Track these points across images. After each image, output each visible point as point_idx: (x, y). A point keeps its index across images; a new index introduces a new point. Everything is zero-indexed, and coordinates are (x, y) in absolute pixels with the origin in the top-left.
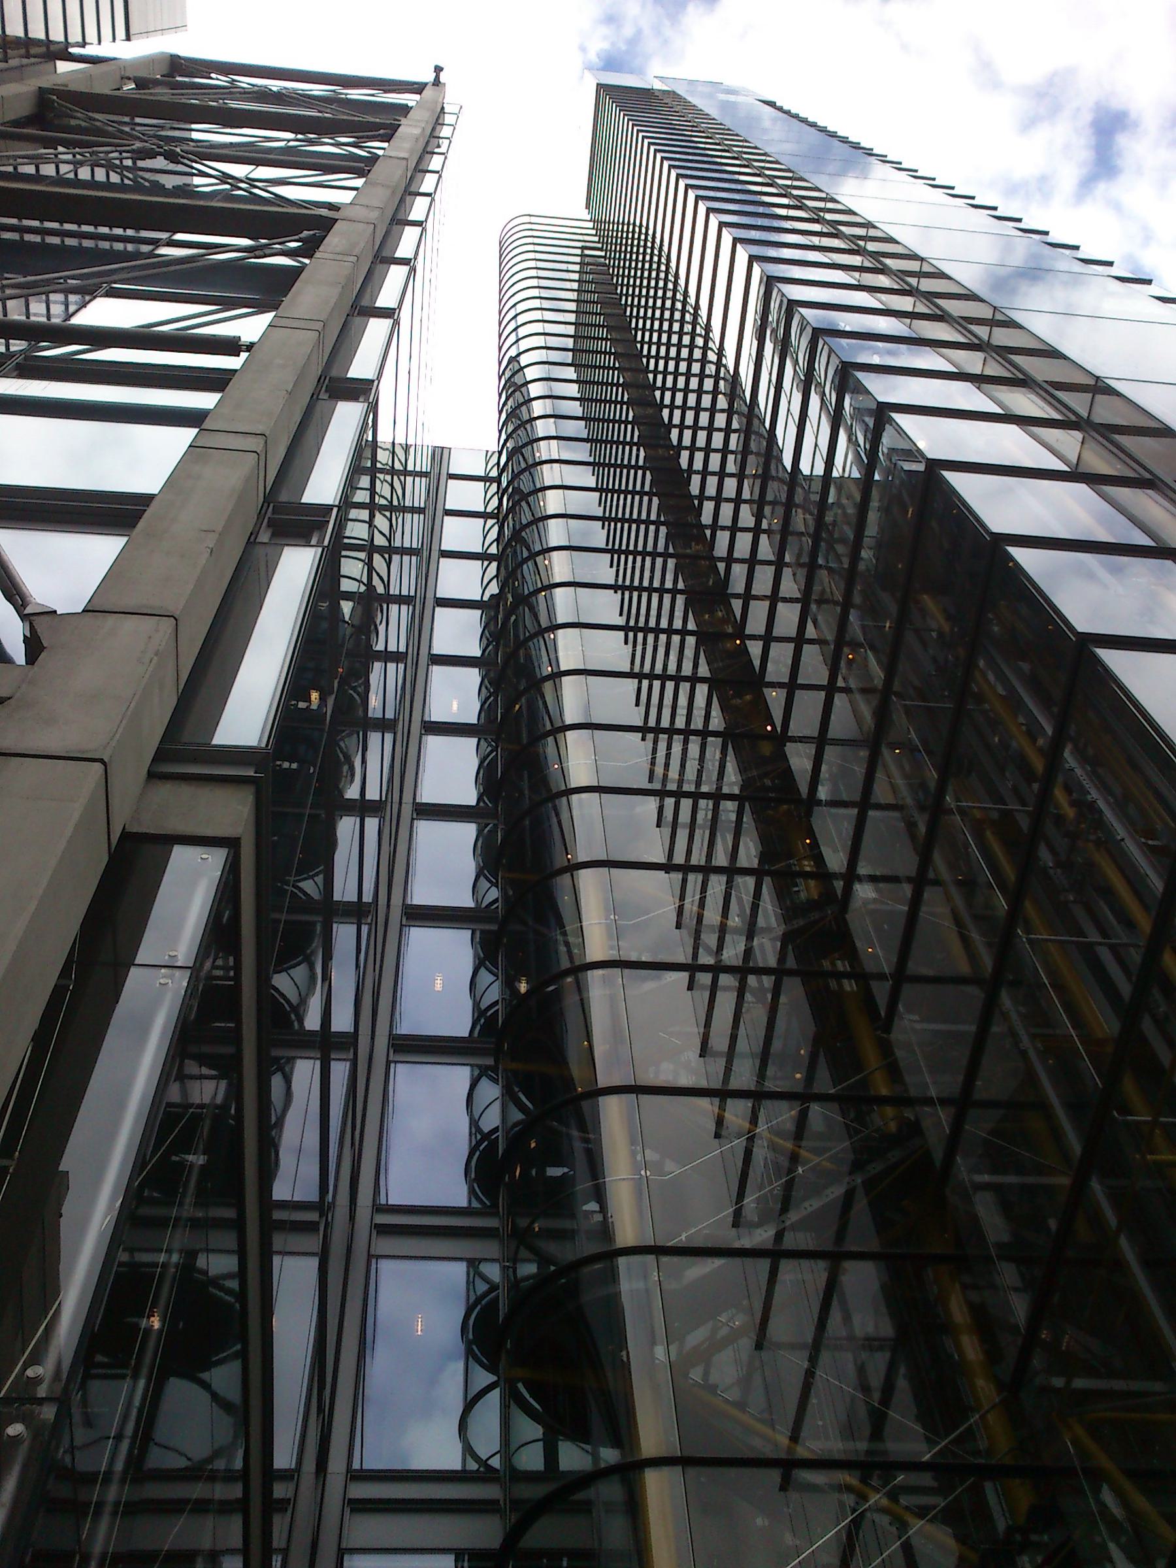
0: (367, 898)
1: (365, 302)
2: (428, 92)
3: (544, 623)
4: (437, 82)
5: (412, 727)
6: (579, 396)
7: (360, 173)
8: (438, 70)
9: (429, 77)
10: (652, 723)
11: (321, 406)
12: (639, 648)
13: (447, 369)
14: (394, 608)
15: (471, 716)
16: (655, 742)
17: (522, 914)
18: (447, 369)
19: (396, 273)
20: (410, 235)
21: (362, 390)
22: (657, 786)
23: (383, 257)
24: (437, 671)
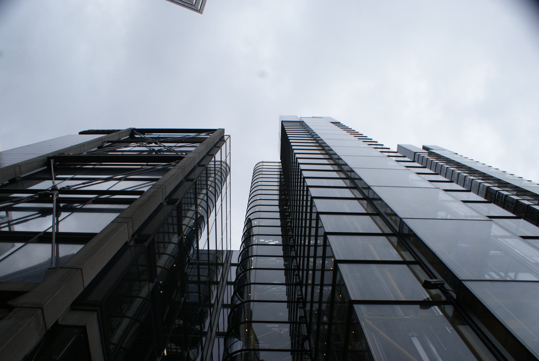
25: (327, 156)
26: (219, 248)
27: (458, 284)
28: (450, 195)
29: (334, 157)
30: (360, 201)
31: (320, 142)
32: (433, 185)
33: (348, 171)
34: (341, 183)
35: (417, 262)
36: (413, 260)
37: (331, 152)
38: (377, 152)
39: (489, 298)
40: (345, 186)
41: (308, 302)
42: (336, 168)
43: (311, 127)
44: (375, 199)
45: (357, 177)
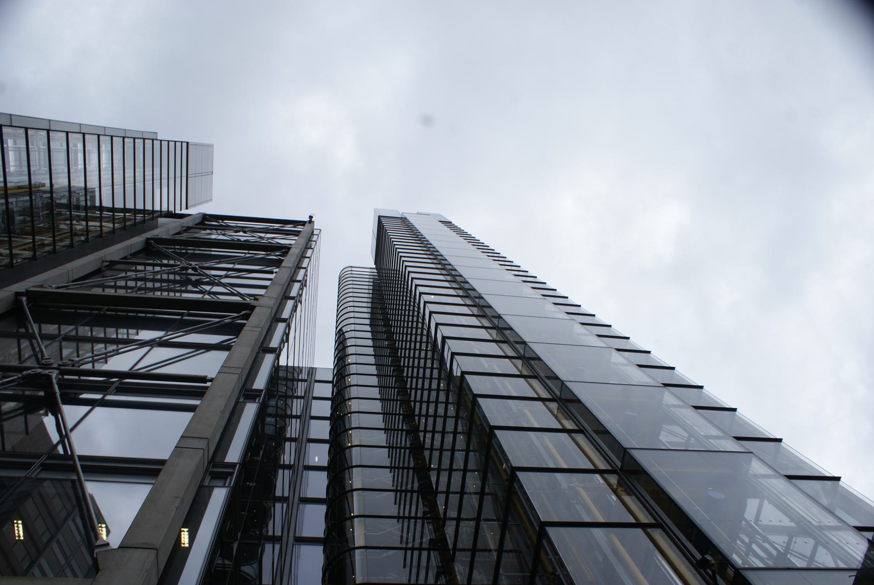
0: (292, 463)
1: (277, 316)
2: (307, 224)
3: (347, 427)
4: (311, 222)
5: (303, 441)
6: (379, 397)
7: (297, 235)
8: (311, 217)
9: (307, 219)
10: (401, 515)
11: (260, 355)
12: (402, 507)
13: (313, 341)
14: (294, 420)
15: (320, 534)
16: (403, 523)
17: (338, 467)
18: (313, 341)
19: (307, 260)
20: (306, 260)
21: (287, 322)
22: (404, 546)
23: (303, 257)
24: (313, 422)
25: (461, 293)
26: (296, 365)
27: (624, 453)
28: (645, 373)
29: (472, 293)
30: (500, 344)
31: (439, 257)
32: (742, 446)
33: (476, 297)
34: (483, 334)
35: (658, 525)
36: (550, 397)
37: (454, 273)
38: (509, 276)
39: (657, 467)
40: (491, 338)
41: (427, 449)
42: (475, 311)
43: (416, 226)
44: (506, 329)
45: (534, 356)
